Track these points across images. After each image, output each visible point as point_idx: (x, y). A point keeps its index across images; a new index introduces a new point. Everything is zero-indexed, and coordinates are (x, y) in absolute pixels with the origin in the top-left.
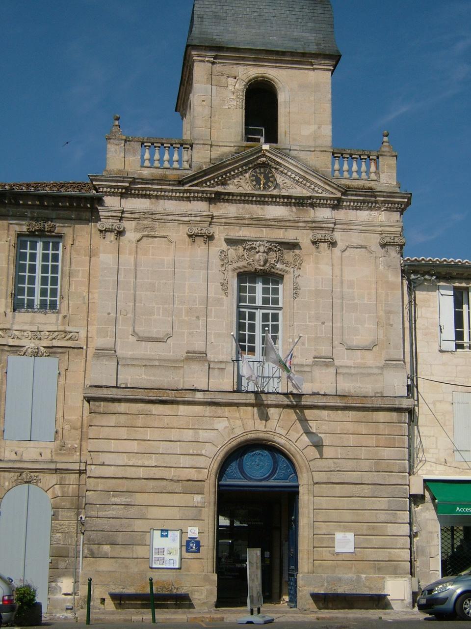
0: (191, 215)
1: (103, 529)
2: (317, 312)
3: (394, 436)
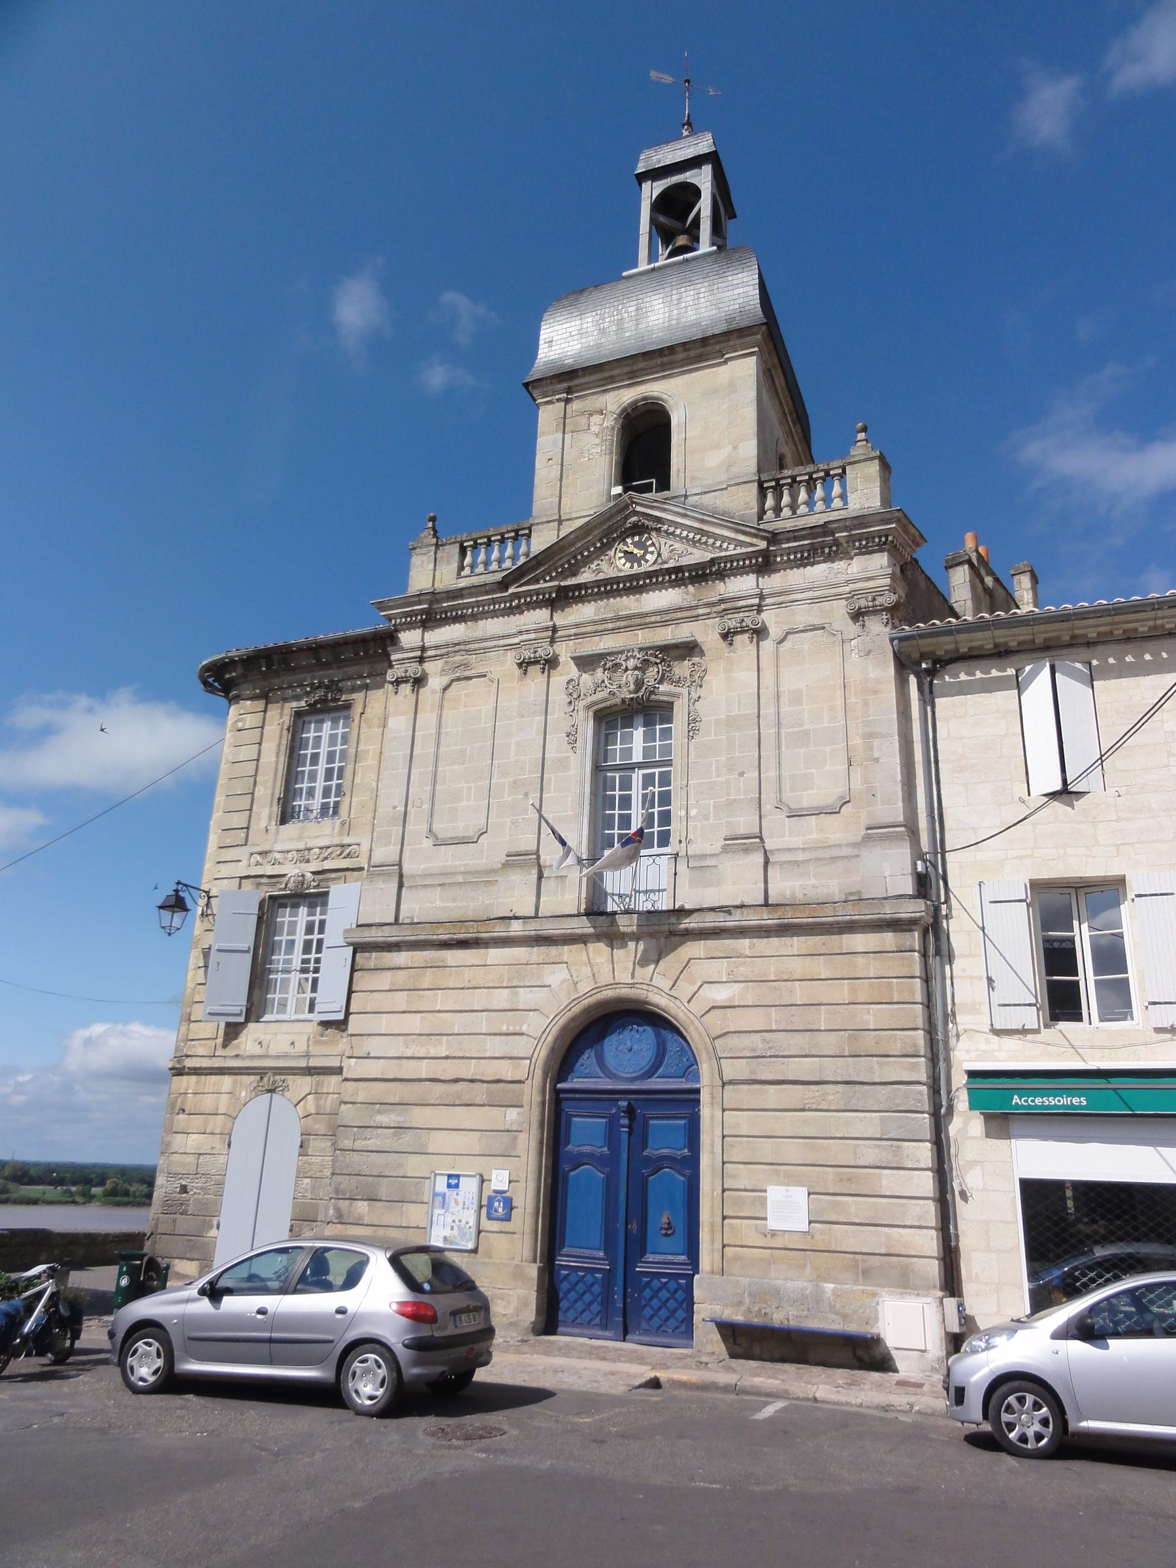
0: (520, 633)
1: (360, 1171)
2: (730, 756)
3: (889, 980)
